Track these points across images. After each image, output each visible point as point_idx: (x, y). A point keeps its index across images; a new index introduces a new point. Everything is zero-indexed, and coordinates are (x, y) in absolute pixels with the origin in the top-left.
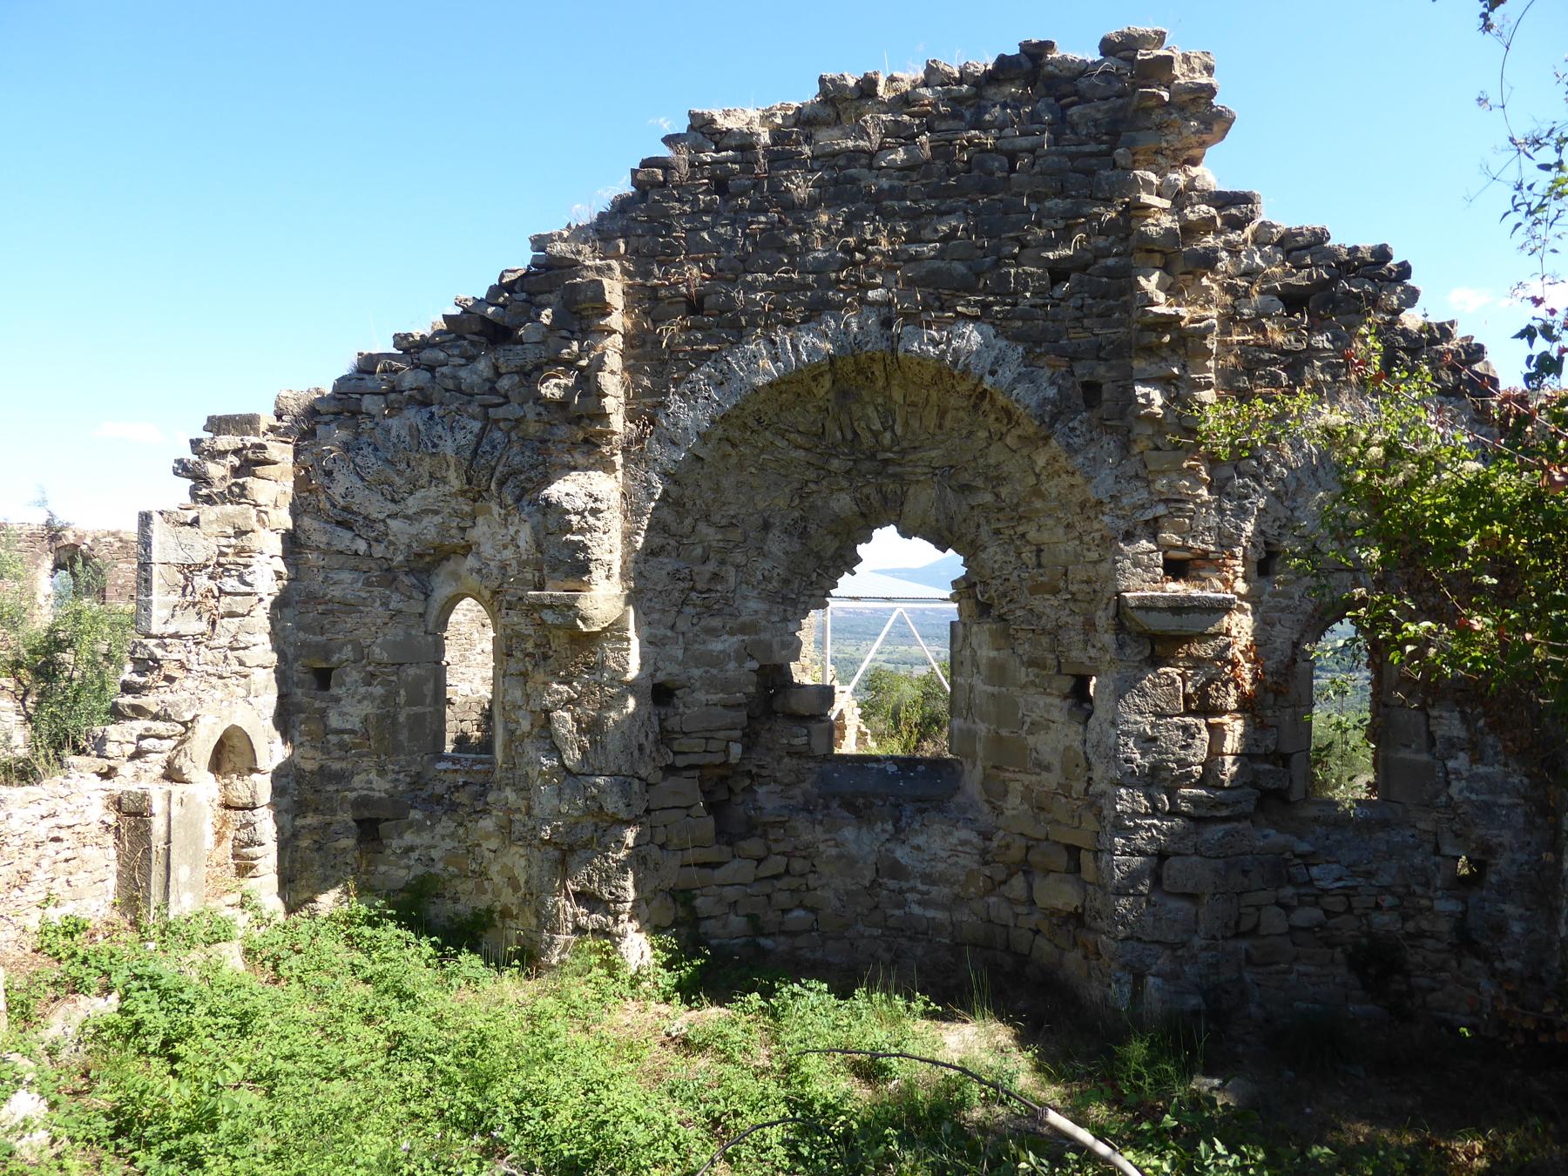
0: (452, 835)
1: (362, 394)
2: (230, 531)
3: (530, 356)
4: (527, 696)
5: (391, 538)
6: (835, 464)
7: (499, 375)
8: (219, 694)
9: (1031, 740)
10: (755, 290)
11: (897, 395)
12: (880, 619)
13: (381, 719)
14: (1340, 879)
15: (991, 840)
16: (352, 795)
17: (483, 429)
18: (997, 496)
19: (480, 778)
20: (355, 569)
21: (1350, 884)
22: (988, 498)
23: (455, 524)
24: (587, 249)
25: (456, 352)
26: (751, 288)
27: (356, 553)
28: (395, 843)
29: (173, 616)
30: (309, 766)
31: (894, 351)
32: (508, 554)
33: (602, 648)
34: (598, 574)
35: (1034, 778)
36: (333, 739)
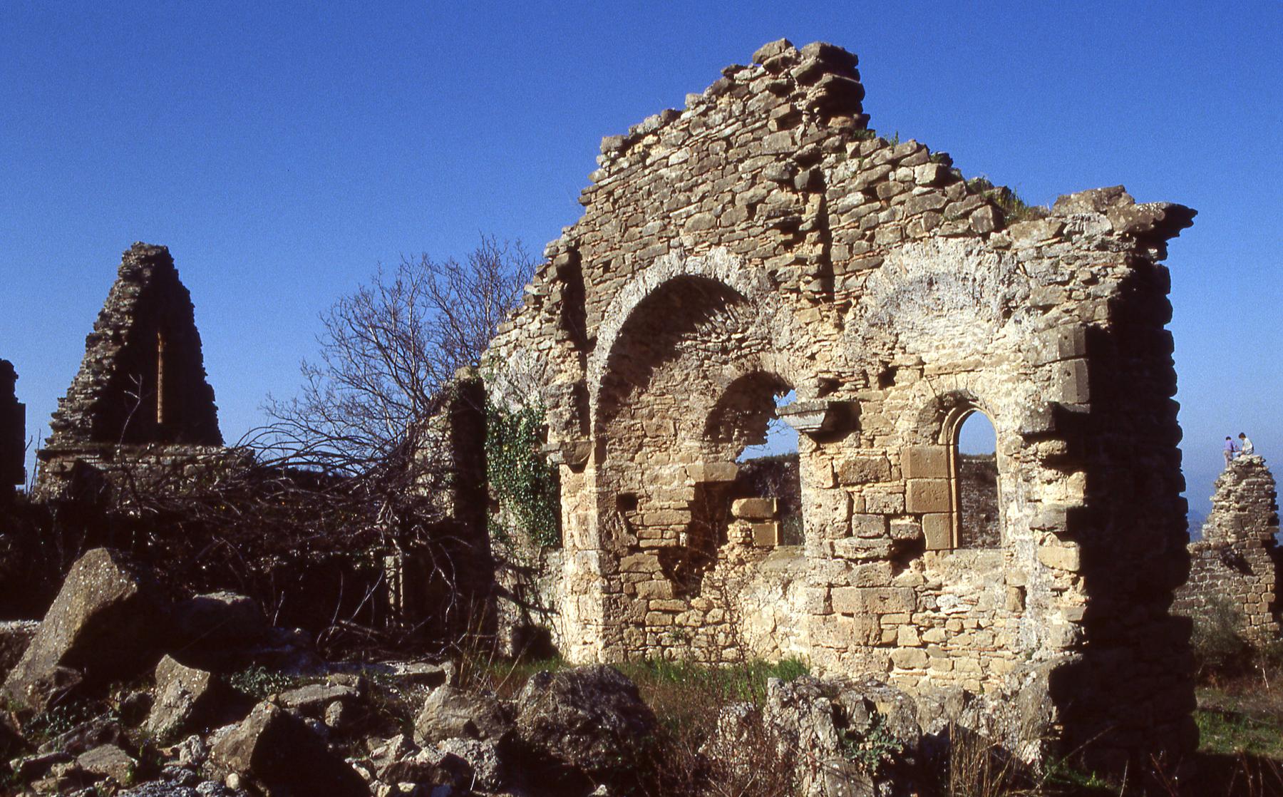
14: (955, 606)
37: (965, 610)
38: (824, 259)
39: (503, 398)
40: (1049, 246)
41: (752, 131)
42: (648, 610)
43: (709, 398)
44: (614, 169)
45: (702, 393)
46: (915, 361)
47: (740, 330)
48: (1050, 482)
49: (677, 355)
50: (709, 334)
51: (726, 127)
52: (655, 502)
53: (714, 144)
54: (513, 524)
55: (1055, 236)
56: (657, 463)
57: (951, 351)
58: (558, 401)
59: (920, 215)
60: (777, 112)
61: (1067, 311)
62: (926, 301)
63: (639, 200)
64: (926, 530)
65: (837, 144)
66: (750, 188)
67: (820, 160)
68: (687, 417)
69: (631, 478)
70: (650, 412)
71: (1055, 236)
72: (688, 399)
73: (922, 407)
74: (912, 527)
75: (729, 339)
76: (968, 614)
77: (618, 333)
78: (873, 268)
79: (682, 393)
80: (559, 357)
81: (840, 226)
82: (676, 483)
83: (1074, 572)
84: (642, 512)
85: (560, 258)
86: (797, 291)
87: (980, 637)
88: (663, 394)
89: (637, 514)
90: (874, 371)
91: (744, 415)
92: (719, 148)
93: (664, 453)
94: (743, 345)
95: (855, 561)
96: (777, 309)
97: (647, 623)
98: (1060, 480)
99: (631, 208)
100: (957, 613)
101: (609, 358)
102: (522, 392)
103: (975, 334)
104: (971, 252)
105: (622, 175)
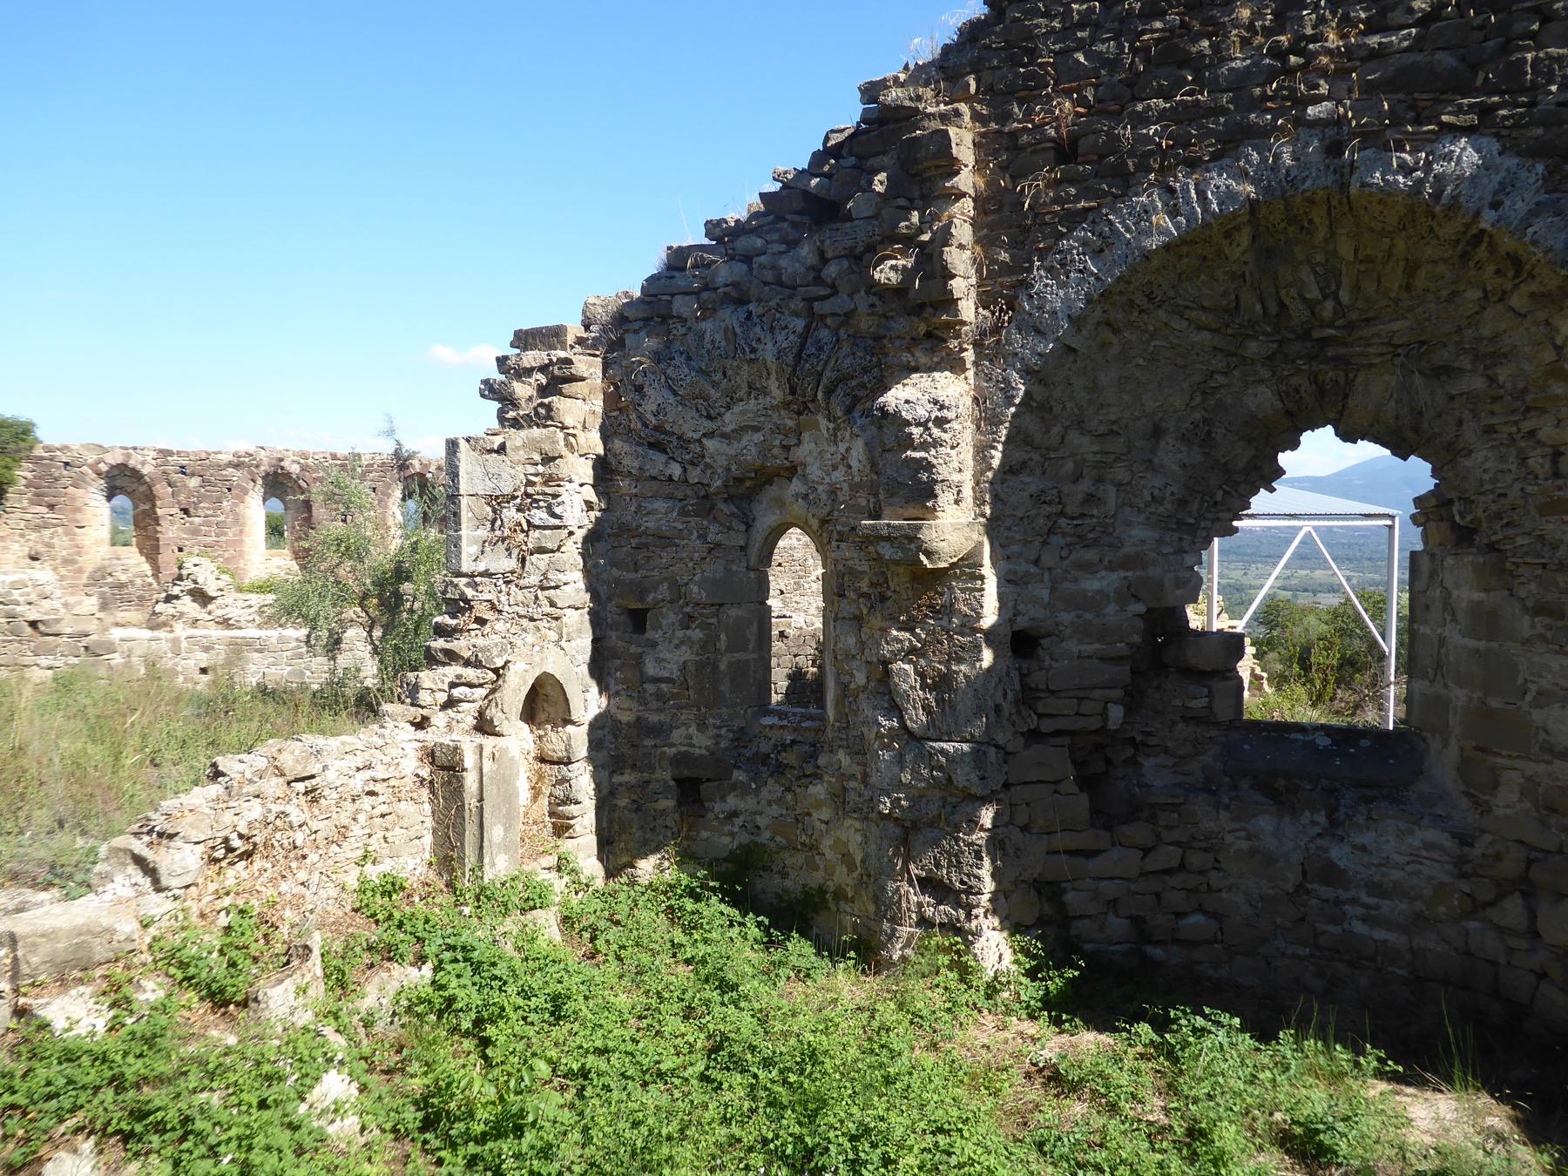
0: (780, 801)
2: (537, 458)
3: (860, 234)
4: (862, 644)
5: (707, 460)
6: (1252, 347)
7: (824, 260)
8: (530, 639)
9: (1537, 716)
10: (1147, 122)
11: (1345, 249)
12: (1286, 538)
13: (700, 666)
15: (1471, 845)
16: (671, 751)
17: (807, 327)
18: (1492, 380)
19: (810, 737)
20: (670, 497)
22: (1478, 383)
23: (777, 442)
24: (928, 93)
25: (776, 236)
26: (1142, 120)
27: (670, 479)
28: (718, 807)
29: (483, 552)
30: (625, 717)
31: (1344, 187)
32: (838, 475)
33: (951, 588)
34: (945, 498)
35: (1541, 768)
36: (650, 688)
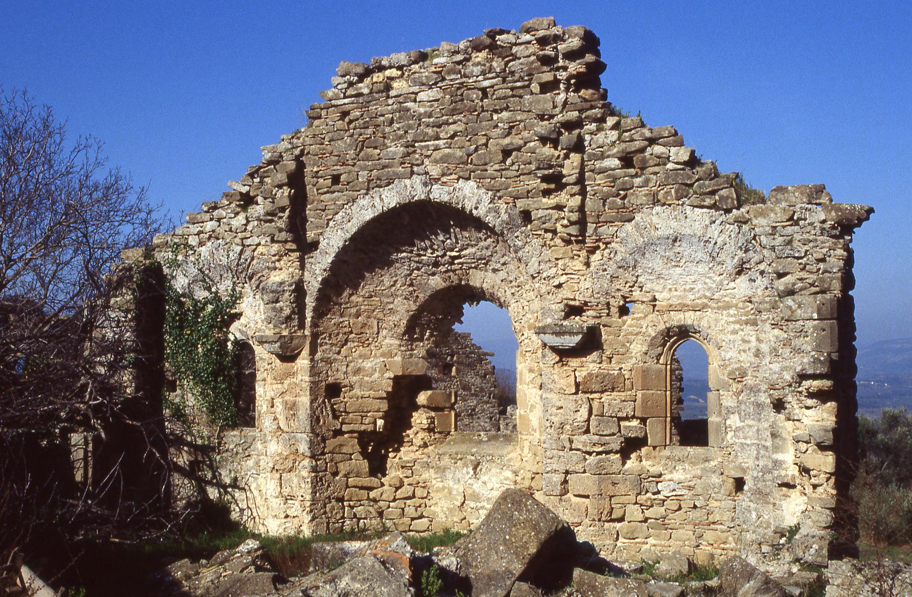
1: (188, 235)
14: (674, 490)
21: (679, 493)
37: (683, 493)
38: (581, 209)
39: (189, 284)
40: (784, 227)
41: (512, 89)
42: (347, 487)
43: (412, 302)
44: (350, 92)
45: (406, 298)
46: (650, 298)
47: (457, 249)
48: (808, 408)
49: (390, 264)
50: (425, 250)
51: (485, 79)
52: (357, 392)
53: (470, 92)
54: (190, 404)
55: (788, 220)
56: (360, 356)
57: (682, 293)
58: (278, 297)
59: (672, 186)
60: (540, 78)
61: (801, 279)
62: (667, 253)
63: (379, 126)
64: (650, 430)
65: (599, 116)
66: (506, 136)
67: (582, 127)
68: (391, 318)
69: (338, 370)
70: (357, 311)
71: (788, 220)
72: (393, 303)
73: (653, 334)
74: (640, 428)
75: (442, 256)
76: (685, 497)
77: (346, 241)
78: (624, 222)
79: (388, 297)
80: (274, 256)
81: (597, 184)
82: (377, 375)
83: (829, 473)
84: (345, 400)
85: (285, 165)
86: (554, 232)
87: (693, 515)
88: (371, 296)
89: (342, 402)
90: (616, 303)
91: (437, 319)
92: (475, 96)
93: (368, 348)
94: (456, 262)
95: (590, 454)
96: (527, 242)
97: (346, 498)
98: (818, 407)
99: (370, 131)
100: (676, 496)
101: (333, 263)
102: (212, 280)
103: (705, 283)
104: (714, 222)
105: (361, 100)
